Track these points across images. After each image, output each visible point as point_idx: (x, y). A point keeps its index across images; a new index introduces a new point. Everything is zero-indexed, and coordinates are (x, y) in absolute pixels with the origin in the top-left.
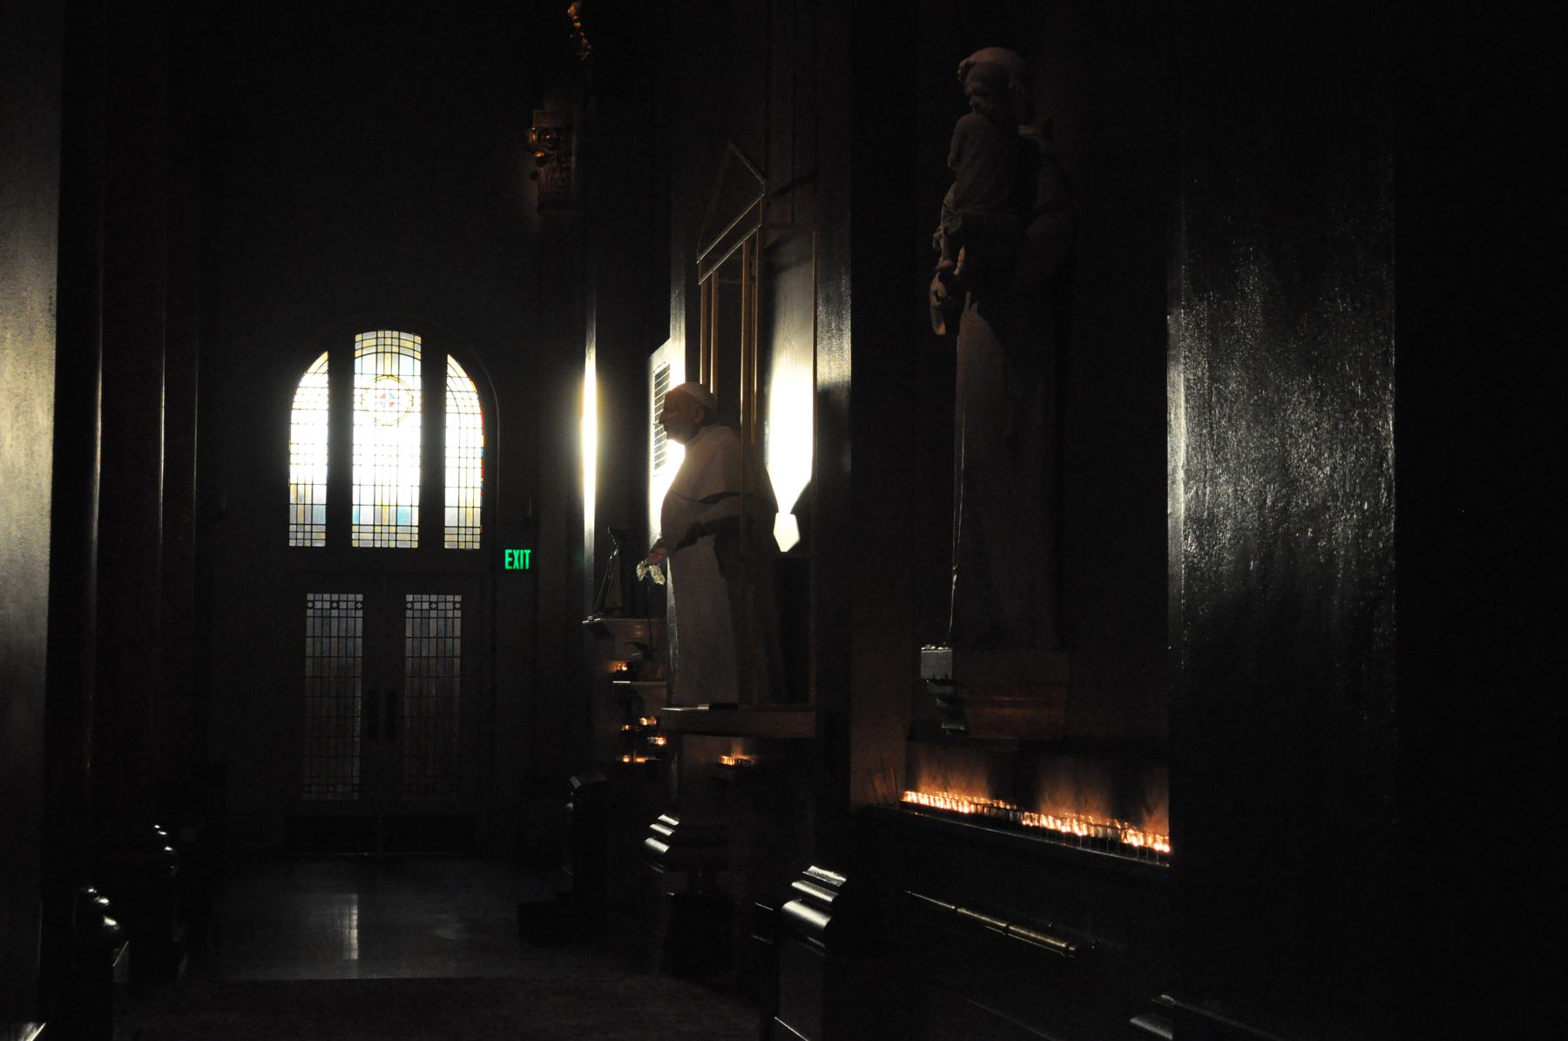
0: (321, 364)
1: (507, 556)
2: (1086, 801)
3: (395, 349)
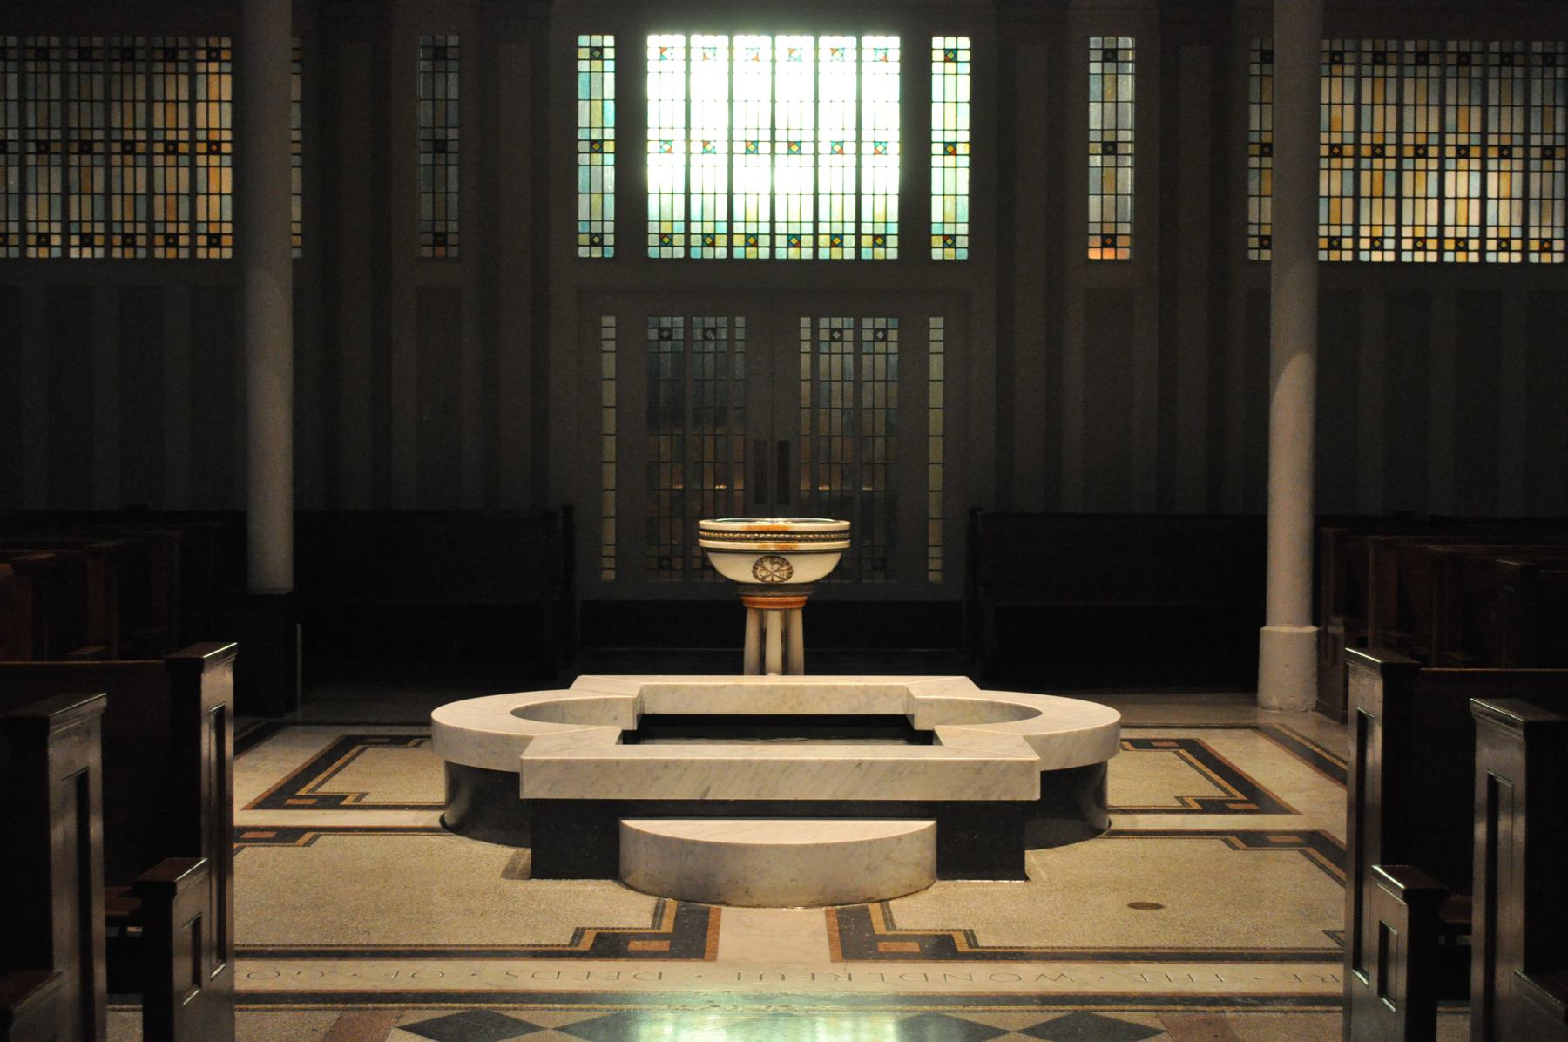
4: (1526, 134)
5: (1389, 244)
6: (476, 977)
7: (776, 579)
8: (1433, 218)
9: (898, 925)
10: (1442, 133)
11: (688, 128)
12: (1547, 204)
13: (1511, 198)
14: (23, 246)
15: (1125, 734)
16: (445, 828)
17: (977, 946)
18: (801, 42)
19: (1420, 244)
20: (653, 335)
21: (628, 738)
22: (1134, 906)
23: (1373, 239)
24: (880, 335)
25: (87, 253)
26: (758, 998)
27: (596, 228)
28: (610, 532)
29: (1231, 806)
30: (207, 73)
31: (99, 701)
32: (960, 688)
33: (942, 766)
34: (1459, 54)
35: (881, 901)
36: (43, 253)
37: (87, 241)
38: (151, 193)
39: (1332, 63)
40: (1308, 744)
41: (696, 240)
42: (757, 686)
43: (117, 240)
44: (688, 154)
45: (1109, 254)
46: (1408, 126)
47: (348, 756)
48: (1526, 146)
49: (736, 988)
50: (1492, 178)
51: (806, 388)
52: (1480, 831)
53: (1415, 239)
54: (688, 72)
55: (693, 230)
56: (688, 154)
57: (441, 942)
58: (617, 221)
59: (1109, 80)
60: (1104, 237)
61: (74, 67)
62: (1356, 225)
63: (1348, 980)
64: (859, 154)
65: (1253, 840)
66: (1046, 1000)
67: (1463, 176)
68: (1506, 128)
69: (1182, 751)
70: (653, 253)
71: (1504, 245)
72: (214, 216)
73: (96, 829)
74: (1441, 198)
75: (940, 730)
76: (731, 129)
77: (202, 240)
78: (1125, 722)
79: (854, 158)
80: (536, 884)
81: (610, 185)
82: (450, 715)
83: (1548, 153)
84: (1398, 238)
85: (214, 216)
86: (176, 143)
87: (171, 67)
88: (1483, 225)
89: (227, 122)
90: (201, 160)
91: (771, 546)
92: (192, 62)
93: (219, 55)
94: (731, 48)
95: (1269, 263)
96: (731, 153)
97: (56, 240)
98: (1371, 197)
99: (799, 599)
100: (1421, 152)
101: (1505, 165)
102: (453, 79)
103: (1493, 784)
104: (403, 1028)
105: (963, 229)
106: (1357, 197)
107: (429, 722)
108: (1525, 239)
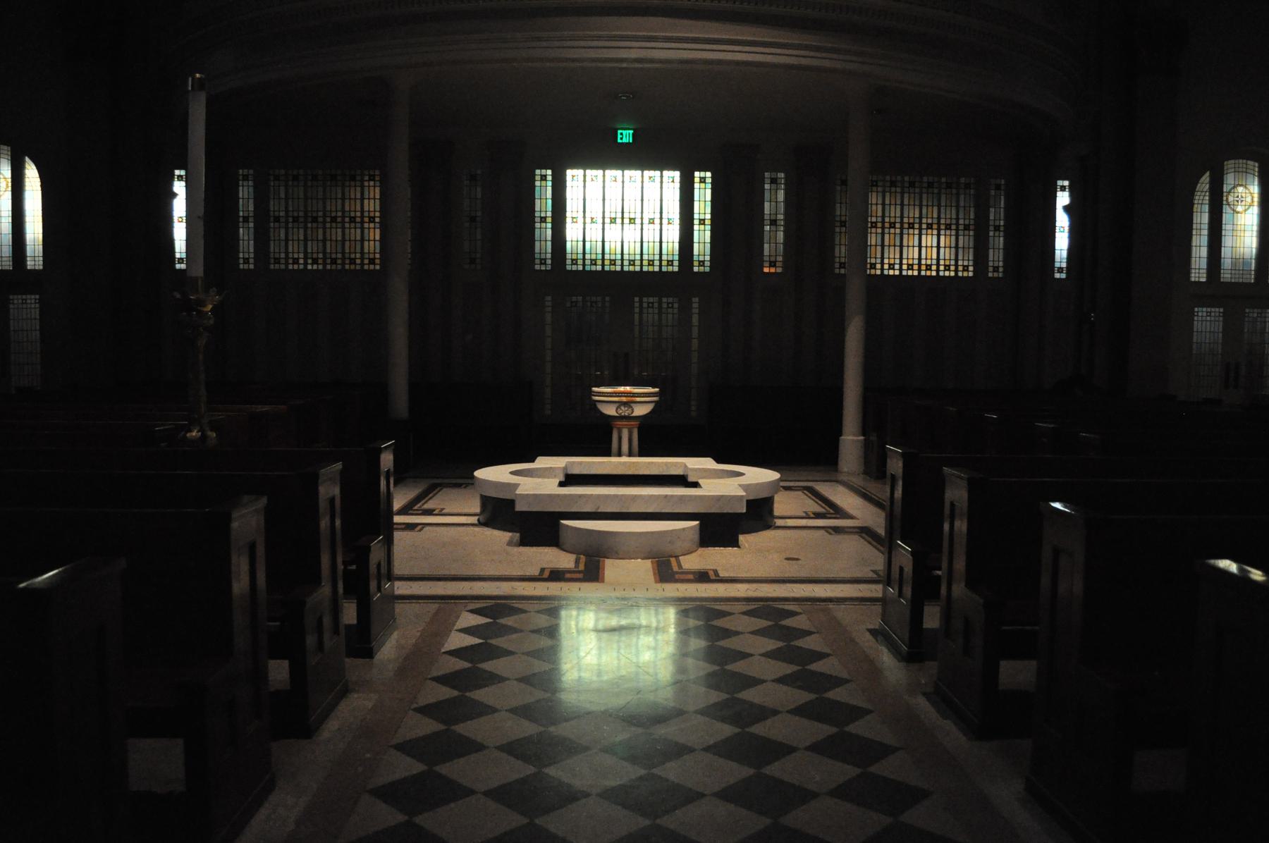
0: (1206, 178)
1: (619, 134)
2: (599, 674)
3: (1244, 170)
4: (957, 219)
5: (897, 267)
6: (498, 589)
7: (626, 414)
8: (916, 256)
9: (684, 567)
10: (921, 218)
11: (584, 212)
12: (966, 251)
13: (950, 247)
14: (287, 264)
15: (782, 484)
16: (480, 524)
17: (718, 576)
18: (636, 174)
19: (910, 267)
20: (568, 304)
21: (562, 484)
22: (787, 559)
23: (890, 264)
24: (670, 305)
25: (315, 267)
26: (624, 599)
27: (543, 256)
28: (548, 392)
29: (829, 516)
30: (369, 186)
31: (339, 466)
32: (708, 463)
33: (701, 497)
34: (929, 183)
35: (675, 557)
36: (296, 267)
37: (315, 261)
38: (344, 240)
39: (872, 186)
40: (861, 489)
41: (588, 262)
42: (618, 462)
43: (329, 261)
44: (585, 223)
45: (773, 270)
46: (906, 215)
47: (435, 492)
48: (957, 224)
49: (613, 594)
50: (942, 238)
51: (637, 329)
52: (946, 527)
53: (908, 265)
54: (585, 187)
55: (625, 258)
56: (585, 223)
57: (481, 573)
58: (552, 253)
59: (773, 192)
60: (770, 262)
61: (290, 183)
62: (882, 258)
63: (884, 591)
64: (661, 224)
65: (837, 530)
66: (748, 600)
67: (929, 237)
68: (948, 216)
69: (805, 492)
70: (569, 268)
71: (947, 268)
72: (372, 251)
73: (338, 523)
74: (920, 247)
75: (701, 481)
76: (604, 212)
77: (366, 261)
78: (784, 478)
79: (659, 226)
80: (522, 549)
81: (549, 238)
82: (483, 474)
83: (967, 228)
84: (901, 264)
85: (372, 251)
86: (355, 217)
87: (353, 183)
88: (938, 259)
89: (378, 208)
90: (366, 225)
91: (624, 399)
92: (362, 181)
93: (374, 178)
94: (604, 176)
95: (845, 275)
96: (604, 223)
97: (301, 261)
98: (889, 246)
99: (636, 423)
100: (911, 226)
101: (948, 232)
102: (479, 189)
103: (952, 504)
104: (468, 611)
105: (708, 258)
106: (883, 246)
107: (473, 477)
108: (956, 265)
